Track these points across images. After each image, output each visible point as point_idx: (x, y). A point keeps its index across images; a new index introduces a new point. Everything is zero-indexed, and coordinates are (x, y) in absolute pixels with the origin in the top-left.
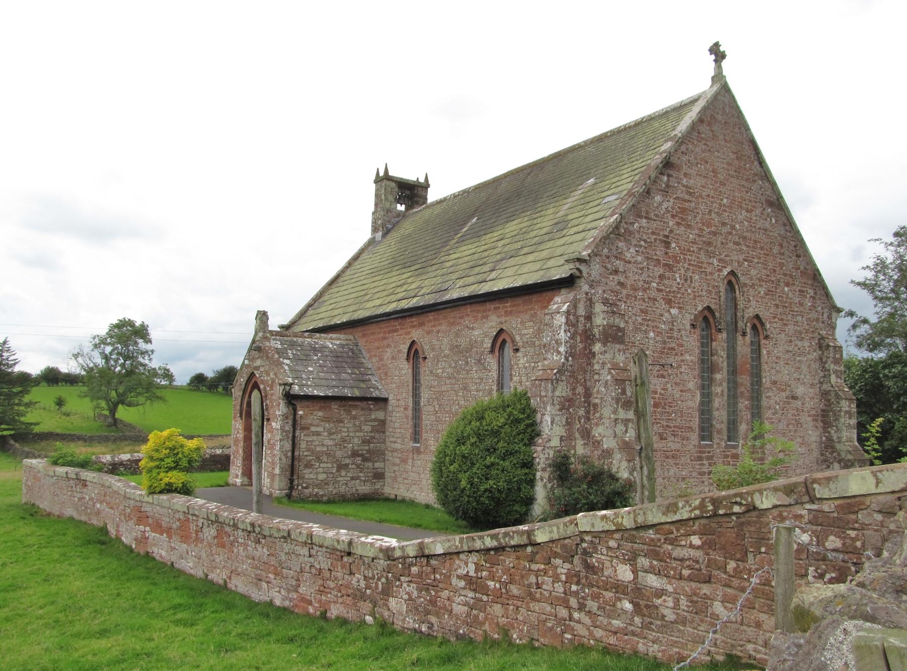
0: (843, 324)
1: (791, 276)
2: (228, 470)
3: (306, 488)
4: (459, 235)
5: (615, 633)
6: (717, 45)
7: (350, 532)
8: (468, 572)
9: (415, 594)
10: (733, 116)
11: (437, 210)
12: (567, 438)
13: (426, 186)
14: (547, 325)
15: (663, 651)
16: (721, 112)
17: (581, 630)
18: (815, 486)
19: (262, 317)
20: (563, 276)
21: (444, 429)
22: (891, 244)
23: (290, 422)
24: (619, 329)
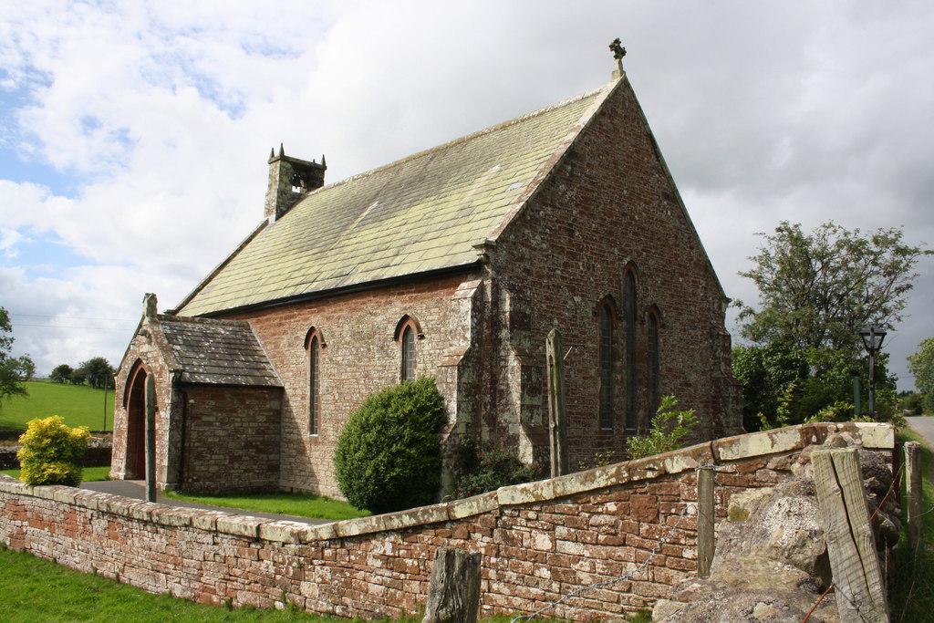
0: (731, 313)
1: (685, 267)
2: (109, 464)
3: (197, 480)
4: (360, 219)
5: (534, 600)
6: (617, 41)
7: (258, 519)
8: (385, 551)
9: (329, 576)
10: (632, 110)
11: (335, 193)
12: (473, 426)
13: (323, 168)
14: (453, 311)
15: (579, 613)
16: (621, 107)
17: (501, 600)
18: (720, 449)
19: (152, 300)
20: (470, 261)
21: (346, 419)
22: (774, 238)
23: (180, 411)
24: (525, 316)
